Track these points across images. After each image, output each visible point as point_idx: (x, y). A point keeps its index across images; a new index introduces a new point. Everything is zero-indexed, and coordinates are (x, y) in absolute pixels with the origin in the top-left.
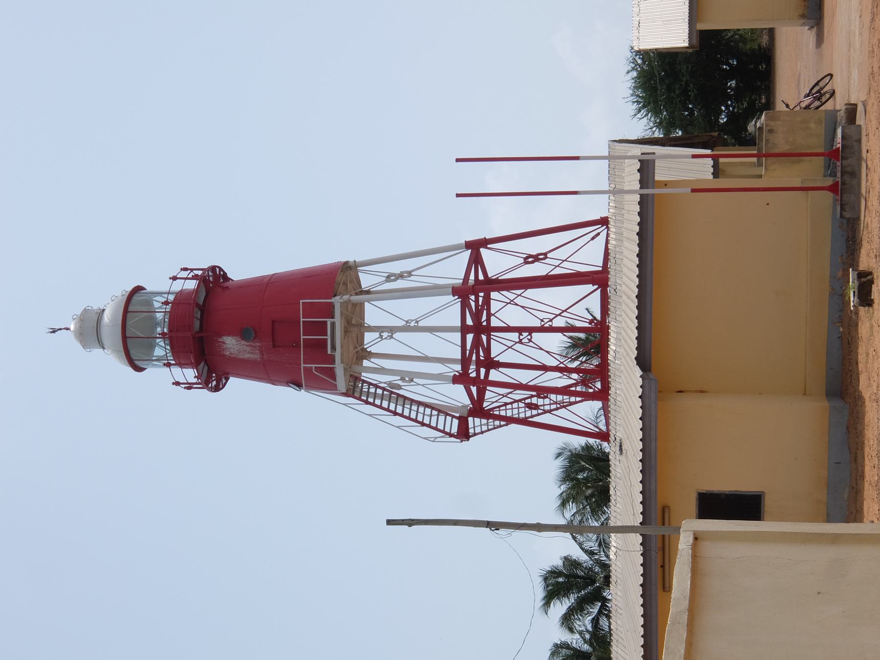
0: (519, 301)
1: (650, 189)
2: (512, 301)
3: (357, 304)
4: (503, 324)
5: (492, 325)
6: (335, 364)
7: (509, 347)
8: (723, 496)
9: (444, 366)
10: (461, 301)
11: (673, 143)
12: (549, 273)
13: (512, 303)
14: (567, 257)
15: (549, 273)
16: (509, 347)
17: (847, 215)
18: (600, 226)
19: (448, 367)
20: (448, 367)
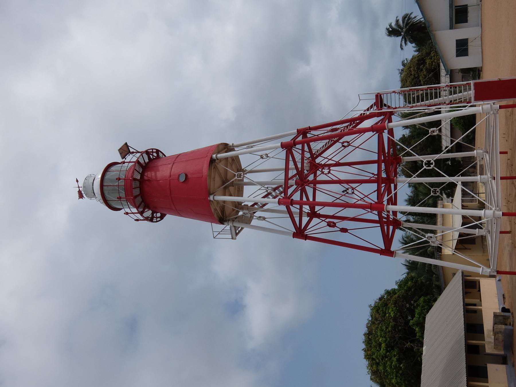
0: (372, 176)
1: (227, 196)
2: (362, 199)
3: (228, 158)
4: (336, 178)
5: (377, 184)
6: (391, 205)
7: (367, 196)
8: (417, 213)
9: (365, 210)
10: (479, 229)
11: (334, 130)
12: (323, 207)
13: (362, 200)
14: (297, 209)
15: (323, 207)
16: (367, 196)
17: (344, 191)
18: (308, 235)
19: (309, 229)
20: (309, 229)
